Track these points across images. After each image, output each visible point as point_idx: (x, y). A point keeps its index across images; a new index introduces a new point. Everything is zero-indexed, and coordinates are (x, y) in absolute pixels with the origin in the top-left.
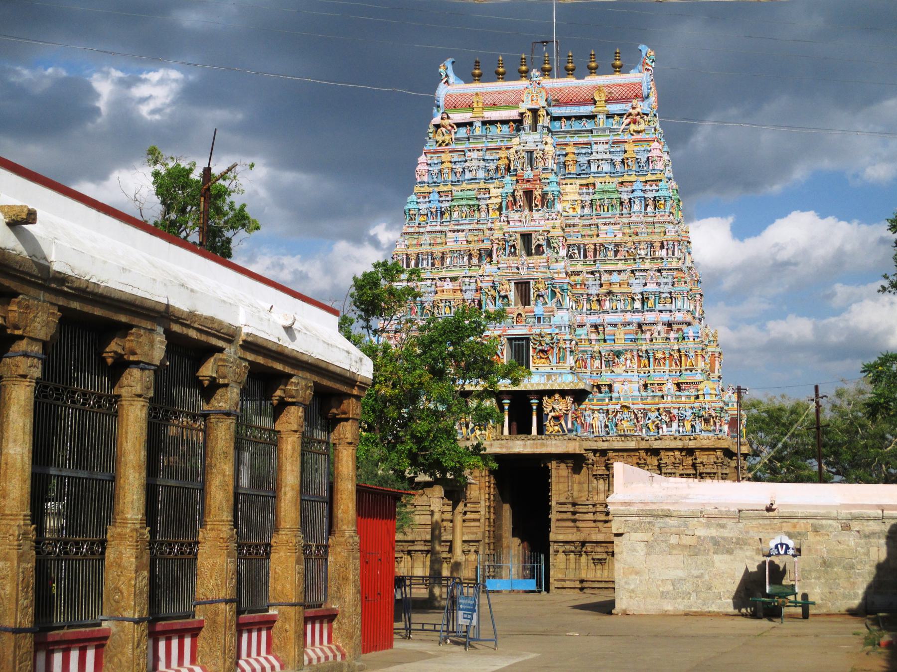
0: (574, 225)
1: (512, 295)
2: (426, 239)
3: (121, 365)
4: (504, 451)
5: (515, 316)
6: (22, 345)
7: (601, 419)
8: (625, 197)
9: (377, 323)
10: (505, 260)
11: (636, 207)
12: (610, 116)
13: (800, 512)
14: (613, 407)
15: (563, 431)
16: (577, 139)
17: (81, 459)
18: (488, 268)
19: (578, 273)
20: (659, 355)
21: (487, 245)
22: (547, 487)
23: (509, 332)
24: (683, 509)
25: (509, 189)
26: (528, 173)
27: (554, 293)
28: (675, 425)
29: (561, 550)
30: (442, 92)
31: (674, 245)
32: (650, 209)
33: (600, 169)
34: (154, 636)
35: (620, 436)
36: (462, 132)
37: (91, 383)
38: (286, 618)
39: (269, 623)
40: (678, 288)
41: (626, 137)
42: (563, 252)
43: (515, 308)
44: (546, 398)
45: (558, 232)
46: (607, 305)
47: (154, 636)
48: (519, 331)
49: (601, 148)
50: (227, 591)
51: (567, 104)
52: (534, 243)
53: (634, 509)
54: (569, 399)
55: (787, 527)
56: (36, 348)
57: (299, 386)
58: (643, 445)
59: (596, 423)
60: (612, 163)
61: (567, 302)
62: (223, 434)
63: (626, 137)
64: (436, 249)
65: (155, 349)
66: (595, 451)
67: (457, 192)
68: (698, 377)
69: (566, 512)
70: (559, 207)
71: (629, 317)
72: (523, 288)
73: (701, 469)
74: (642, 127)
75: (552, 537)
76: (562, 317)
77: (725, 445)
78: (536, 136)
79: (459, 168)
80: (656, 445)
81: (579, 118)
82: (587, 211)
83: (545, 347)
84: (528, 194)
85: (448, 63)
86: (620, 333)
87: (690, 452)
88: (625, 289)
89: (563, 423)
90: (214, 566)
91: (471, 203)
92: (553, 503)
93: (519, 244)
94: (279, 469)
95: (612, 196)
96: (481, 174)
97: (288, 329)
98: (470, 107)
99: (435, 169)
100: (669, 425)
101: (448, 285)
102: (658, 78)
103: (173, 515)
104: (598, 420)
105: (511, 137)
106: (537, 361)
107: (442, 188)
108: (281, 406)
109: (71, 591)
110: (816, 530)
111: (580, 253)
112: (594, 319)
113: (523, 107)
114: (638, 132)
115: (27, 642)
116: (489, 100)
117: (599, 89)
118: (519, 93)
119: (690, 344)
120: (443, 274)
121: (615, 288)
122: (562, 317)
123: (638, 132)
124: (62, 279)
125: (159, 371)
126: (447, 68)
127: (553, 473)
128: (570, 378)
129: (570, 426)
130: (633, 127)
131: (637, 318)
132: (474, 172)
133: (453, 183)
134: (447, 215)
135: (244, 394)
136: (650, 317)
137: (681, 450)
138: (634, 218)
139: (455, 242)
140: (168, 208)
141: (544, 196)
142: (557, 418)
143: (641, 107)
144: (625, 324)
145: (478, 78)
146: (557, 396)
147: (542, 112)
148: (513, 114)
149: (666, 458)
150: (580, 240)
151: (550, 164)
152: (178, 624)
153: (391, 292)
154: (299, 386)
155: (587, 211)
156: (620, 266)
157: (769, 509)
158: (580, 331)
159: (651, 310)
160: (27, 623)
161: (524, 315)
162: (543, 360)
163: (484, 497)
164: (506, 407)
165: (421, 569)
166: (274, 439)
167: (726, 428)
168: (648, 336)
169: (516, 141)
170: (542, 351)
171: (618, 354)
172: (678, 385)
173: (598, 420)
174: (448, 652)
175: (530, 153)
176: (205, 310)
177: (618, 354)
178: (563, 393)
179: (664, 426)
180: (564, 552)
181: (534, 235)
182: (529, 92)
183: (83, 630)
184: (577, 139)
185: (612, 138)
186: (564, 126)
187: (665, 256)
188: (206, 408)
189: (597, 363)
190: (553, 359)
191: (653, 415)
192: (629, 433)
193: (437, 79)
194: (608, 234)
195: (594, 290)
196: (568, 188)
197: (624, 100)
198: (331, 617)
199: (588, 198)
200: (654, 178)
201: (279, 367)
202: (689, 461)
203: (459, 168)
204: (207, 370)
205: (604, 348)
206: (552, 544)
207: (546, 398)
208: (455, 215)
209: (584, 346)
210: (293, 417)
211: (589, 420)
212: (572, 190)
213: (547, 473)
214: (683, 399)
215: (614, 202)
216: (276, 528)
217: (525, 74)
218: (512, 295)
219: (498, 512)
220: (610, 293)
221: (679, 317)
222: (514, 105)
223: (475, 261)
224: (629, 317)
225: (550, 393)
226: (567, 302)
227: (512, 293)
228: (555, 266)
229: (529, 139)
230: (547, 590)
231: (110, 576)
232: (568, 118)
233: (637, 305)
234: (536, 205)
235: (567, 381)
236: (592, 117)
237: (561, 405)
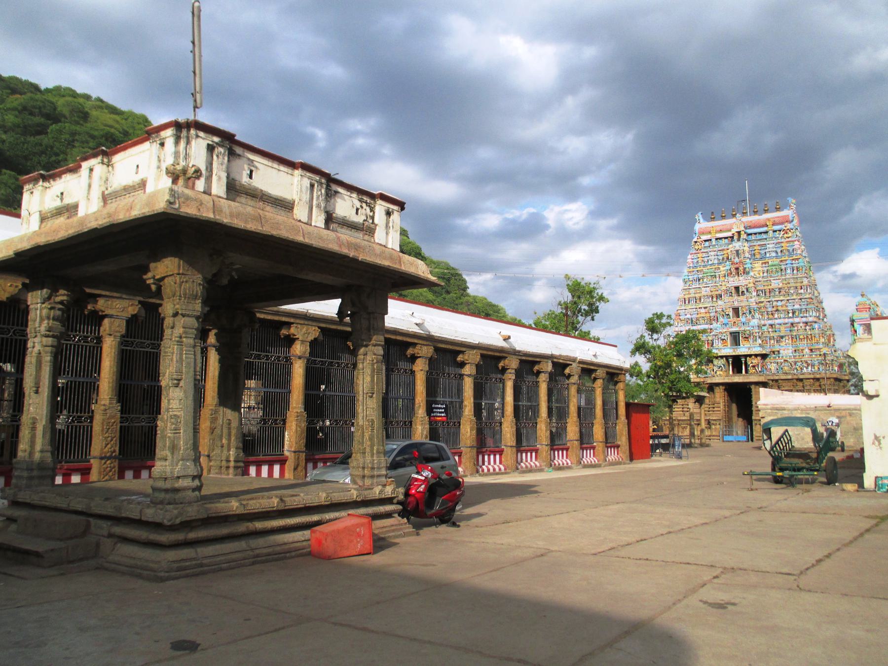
1: (731, 314)
2: (692, 291)
3: (539, 373)
4: (730, 381)
6: (509, 371)
8: (783, 267)
9: (655, 336)
10: (726, 298)
11: (789, 271)
12: (775, 231)
13: (843, 407)
16: (759, 243)
17: (529, 400)
18: (720, 302)
19: (762, 302)
20: (801, 337)
21: (719, 292)
24: (790, 407)
25: (728, 268)
26: (737, 260)
27: (750, 312)
28: (810, 368)
30: (697, 227)
32: (795, 272)
34: (553, 449)
36: (707, 244)
37: (530, 378)
38: (599, 445)
39: (594, 448)
40: (809, 306)
41: (783, 240)
42: (754, 294)
43: (733, 319)
45: (752, 285)
46: (776, 316)
47: (553, 449)
49: (771, 246)
50: (577, 436)
51: (755, 227)
53: (769, 407)
54: (759, 358)
55: (837, 414)
56: (513, 371)
57: (600, 373)
58: (795, 377)
59: (773, 368)
60: (777, 252)
61: (757, 315)
62: (573, 390)
63: (783, 240)
64: (697, 295)
65: (549, 367)
66: (773, 380)
67: (705, 270)
68: (821, 346)
70: (752, 274)
71: (786, 320)
72: (736, 311)
73: (823, 387)
74: (790, 235)
75: (753, 418)
76: (755, 322)
77: (835, 376)
78: (740, 243)
79: (706, 259)
80: (801, 377)
81: (760, 233)
82: (765, 274)
84: (737, 269)
85: (699, 214)
87: (818, 379)
88: (784, 308)
90: (572, 430)
93: (733, 291)
94: (595, 399)
96: (716, 261)
97: (595, 356)
98: (710, 233)
99: (695, 261)
100: (807, 368)
101: (703, 311)
102: (798, 212)
103: (558, 413)
104: (773, 367)
105: (729, 244)
107: (699, 269)
108: (595, 379)
109: (527, 436)
110: (850, 415)
112: (770, 322)
113: (734, 231)
115: (514, 449)
116: (719, 229)
117: (769, 220)
118: (732, 225)
119: (816, 331)
121: (779, 308)
122: (755, 322)
124: (519, 352)
125: (551, 374)
126: (699, 216)
127: (753, 390)
128: (759, 349)
130: (786, 235)
131: (791, 320)
133: (704, 266)
135: (580, 376)
136: (796, 320)
137: (813, 379)
138: (788, 276)
139: (705, 291)
140: (573, 296)
141: (745, 269)
142: (754, 366)
143: (789, 226)
144: (785, 324)
145: (713, 219)
147: (742, 233)
148: (729, 234)
149: (806, 383)
150: (762, 288)
151: (747, 255)
152: (561, 447)
153: (660, 324)
154: (600, 373)
155: (765, 274)
156: (782, 298)
157: (829, 406)
158: (764, 328)
160: (514, 444)
163: (721, 401)
165: (687, 432)
166: (593, 390)
167: (836, 368)
169: (730, 246)
171: (782, 337)
172: (811, 350)
175: (737, 251)
176: (564, 353)
177: (782, 337)
178: (756, 356)
182: (736, 224)
184: (759, 243)
185: (776, 241)
186: (753, 237)
188: (567, 382)
189: (772, 341)
190: (751, 340)
193: (695, 221)
194: (775, 284)
195: (770, 310)
196: (756, 265)
197: (782, 223)
198: (618, 447)
199: (765, 269)
201: (592, 367)
202: (818, 383)
203: (706, 259)
204: (567, 371)
205: (775, 335)
209: (766, 334)
210: (599, 382)
211: (769, 367)
212: (758, 266)
213: (750, 390)
216: (595, 418)
217: (734, 216)
218: (731, 314)
219: (729, 407)
220: (777, 310)
221: (811, 319)
222: (730, 230)
223: (715, 299)
224: (786, 320)
225: (750, 356)
226: (757, 315)
228: (752, 300)
229: (737, 245)
230: (752, 440)
231: (538, 432)
232: (755, 234)
233: (791, 315)
235: (757, 350)
236: (766, 232)
237: (755, 361)
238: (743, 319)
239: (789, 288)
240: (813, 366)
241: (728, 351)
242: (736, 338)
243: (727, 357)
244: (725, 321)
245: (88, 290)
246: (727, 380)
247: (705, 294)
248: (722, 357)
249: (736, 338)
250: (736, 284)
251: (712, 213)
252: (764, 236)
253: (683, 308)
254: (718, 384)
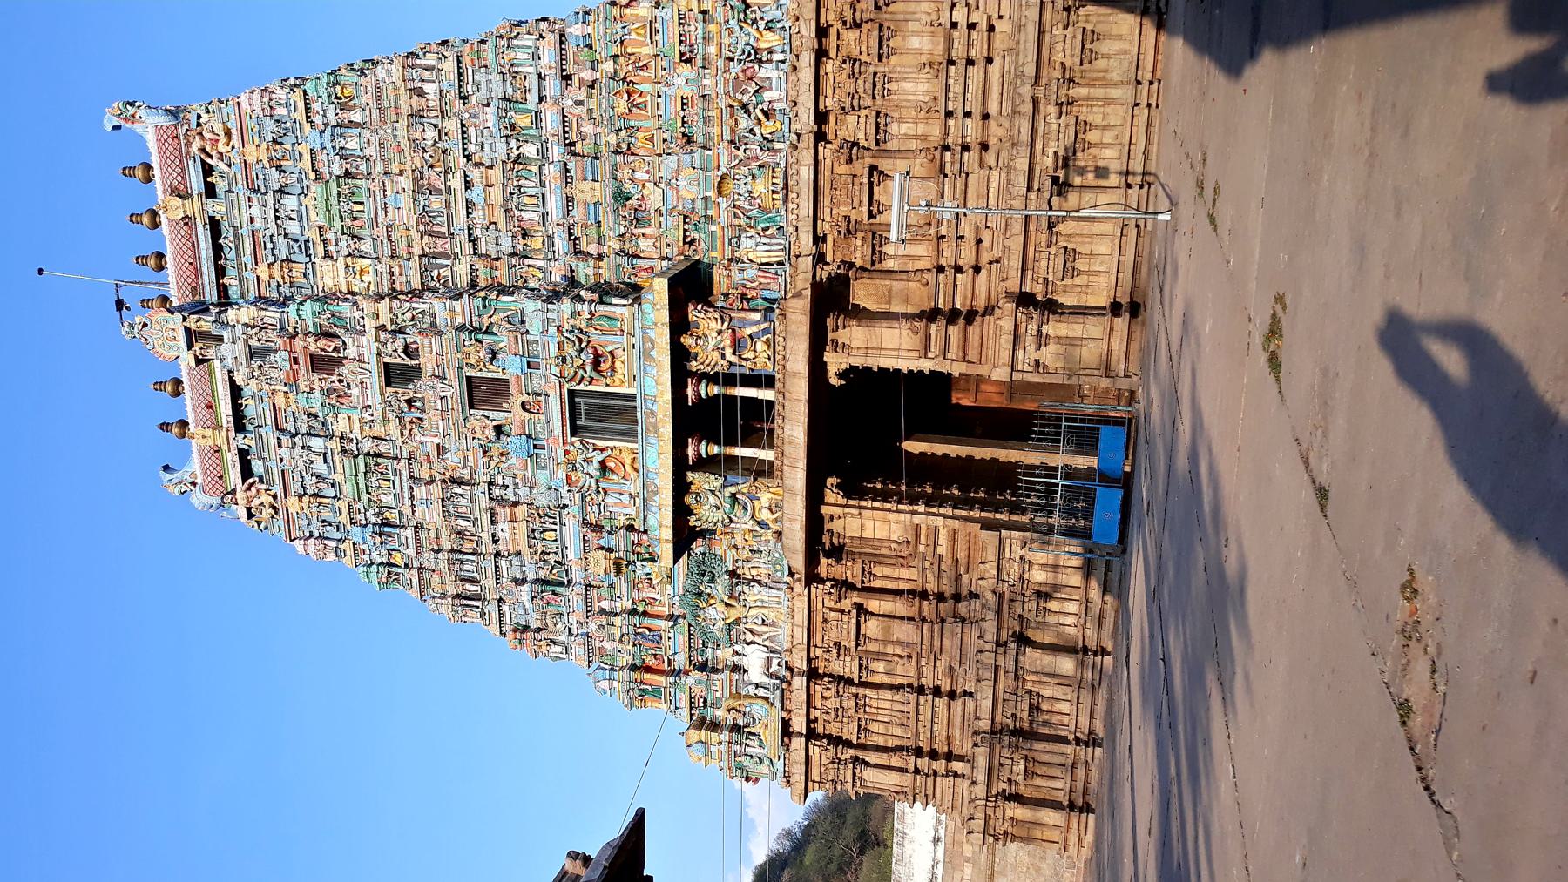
0: (392, 274)
4: (802, 464)
5: (527, 415)
7: (751, 243)
12: (210, 191)
14: (723, 214)
15: (765, 331)
22: (889, 377)
23: (557, 430)
29: (1033, 354)
31: (412, 67)
33: (294, 215)
35: (786, 200)
43: (512, 414)
44: (694, 366)
48: (555, 410)
51: (198, 274)
52: (400, 359)
54: (695, 313)
69: (947, 338)
74: (218, 128)
80: (807, 118)
82: (366, 247)
83: (588, 358)
86: (585, 191)
89: (748, 331)
91: (362, 468)
92: (927, 366)
95: (335, 193)
106: (618, 376)
111: (439, 267)
114: (228, 134)
120: (486, 538)
123: (228, 134)
129: (757, 316)
132: (313, 457)
134: (392, 516)
138: (372, 151)
142: (737, 345)
146: (687, 340)
156: (457, 183)
159: (537, 119)
161: (525, 398)
162: (618, 365)
164: (715, 449)
168: (588, 129)
170: (596, 364)
171: (621, 197)
173: (757, 249)
174: (1240, 546)
177: (621, 197)
178: (679, 325)
179: (767, 96)
180: (1038, 348)
181: (387, 360)
183: (1173, 763)
187: (435, 86)
191: (744, 123)
192: (780, 181)
200: (301, 105)
206: (1017, 377)
207: (694, 366)
208: (388, 500)
214: (712, 49)
215: (345, 190)
224: (552, 171)
225: (680, 356)
227: (491, 414)
234: (336, 349)
236: (215, 226)
237: (708, 327)
238: (510, 367)
239: (417, 146)
240: (756, 56)
241: (656, 450)
242: (598, 415)
243: (681, 466)
244: (515, 444)
245: (913, 447)
246: (797, 477)
247: (437, 508)
248: (681, 487)
249: (598, 415)
250: (374, 379)
251: (165, 427)
252: (226, 230)
253: (492, 609)
254: (815, 524)
